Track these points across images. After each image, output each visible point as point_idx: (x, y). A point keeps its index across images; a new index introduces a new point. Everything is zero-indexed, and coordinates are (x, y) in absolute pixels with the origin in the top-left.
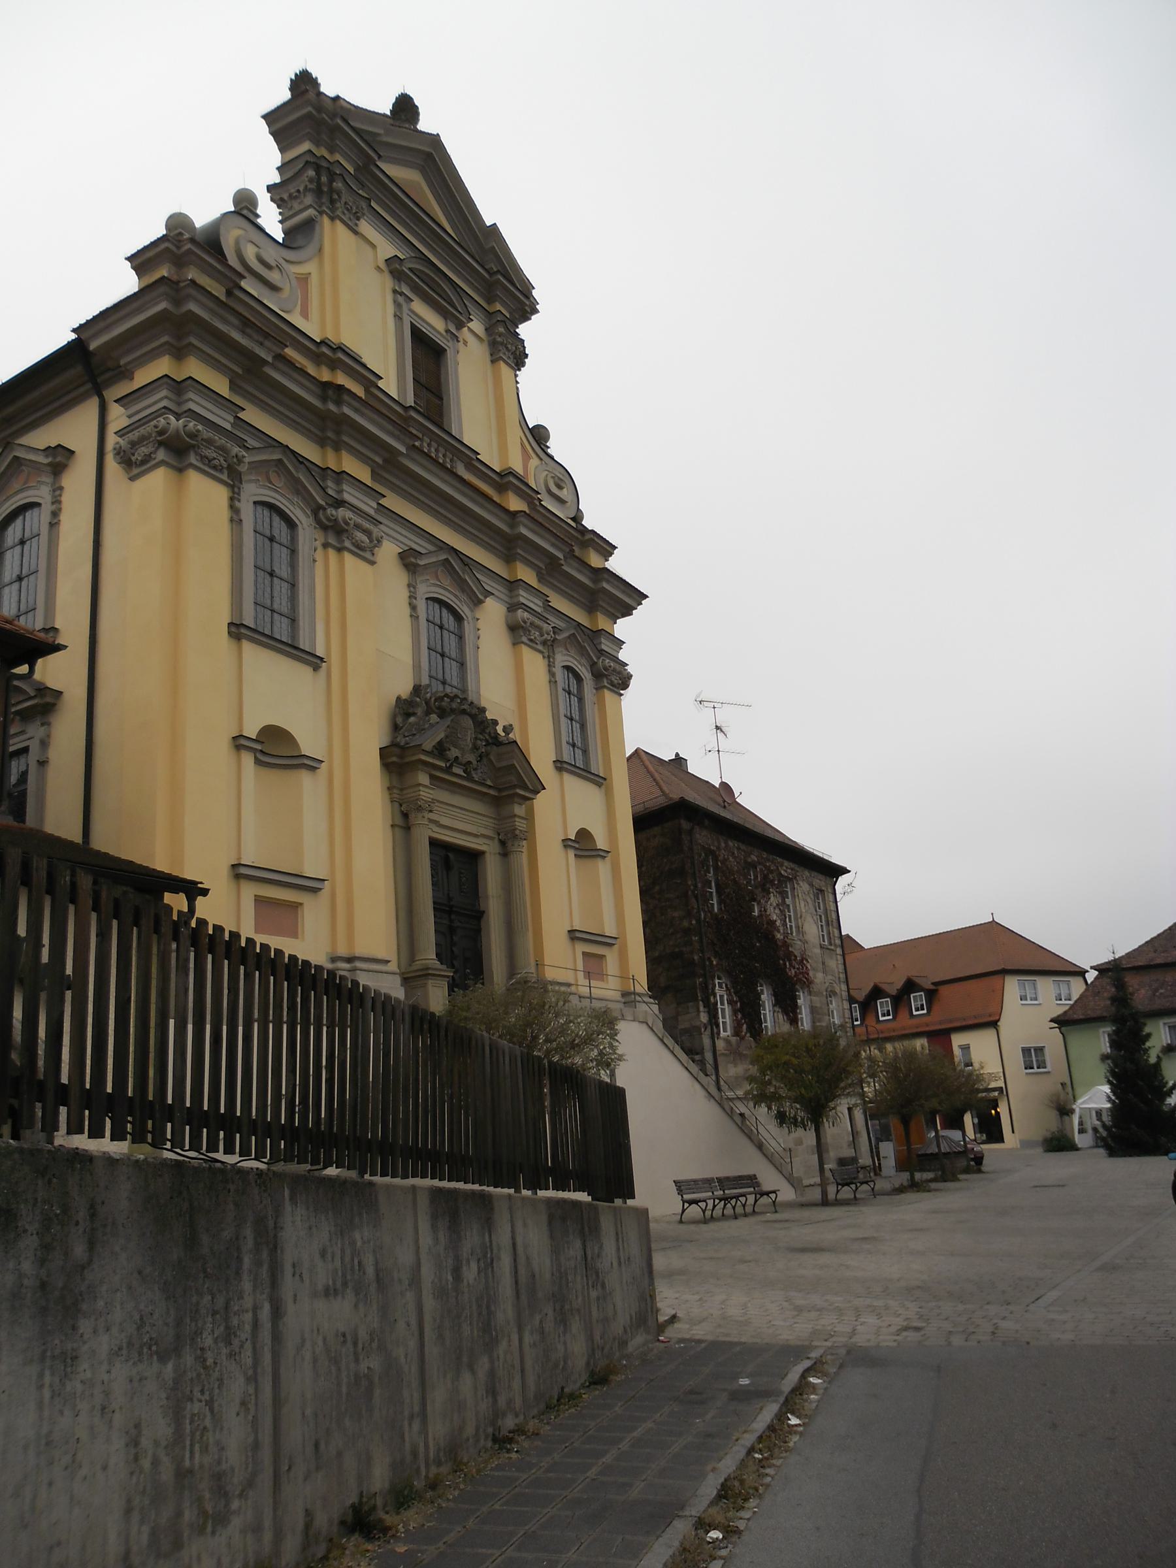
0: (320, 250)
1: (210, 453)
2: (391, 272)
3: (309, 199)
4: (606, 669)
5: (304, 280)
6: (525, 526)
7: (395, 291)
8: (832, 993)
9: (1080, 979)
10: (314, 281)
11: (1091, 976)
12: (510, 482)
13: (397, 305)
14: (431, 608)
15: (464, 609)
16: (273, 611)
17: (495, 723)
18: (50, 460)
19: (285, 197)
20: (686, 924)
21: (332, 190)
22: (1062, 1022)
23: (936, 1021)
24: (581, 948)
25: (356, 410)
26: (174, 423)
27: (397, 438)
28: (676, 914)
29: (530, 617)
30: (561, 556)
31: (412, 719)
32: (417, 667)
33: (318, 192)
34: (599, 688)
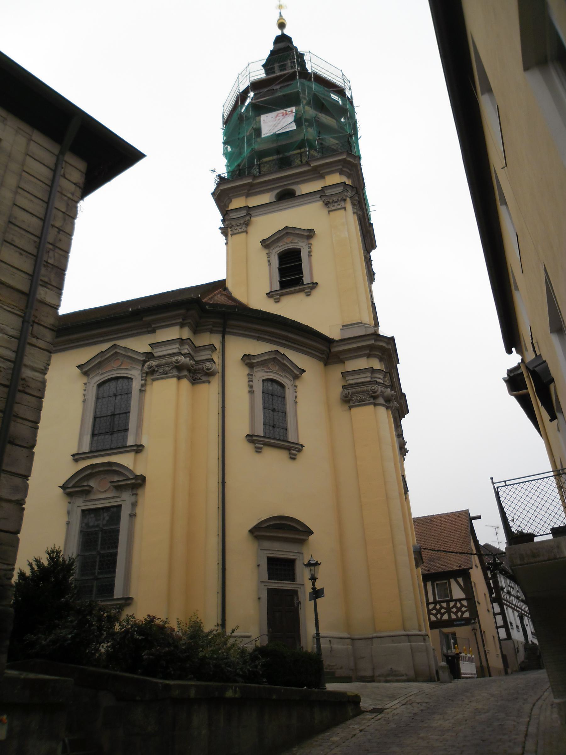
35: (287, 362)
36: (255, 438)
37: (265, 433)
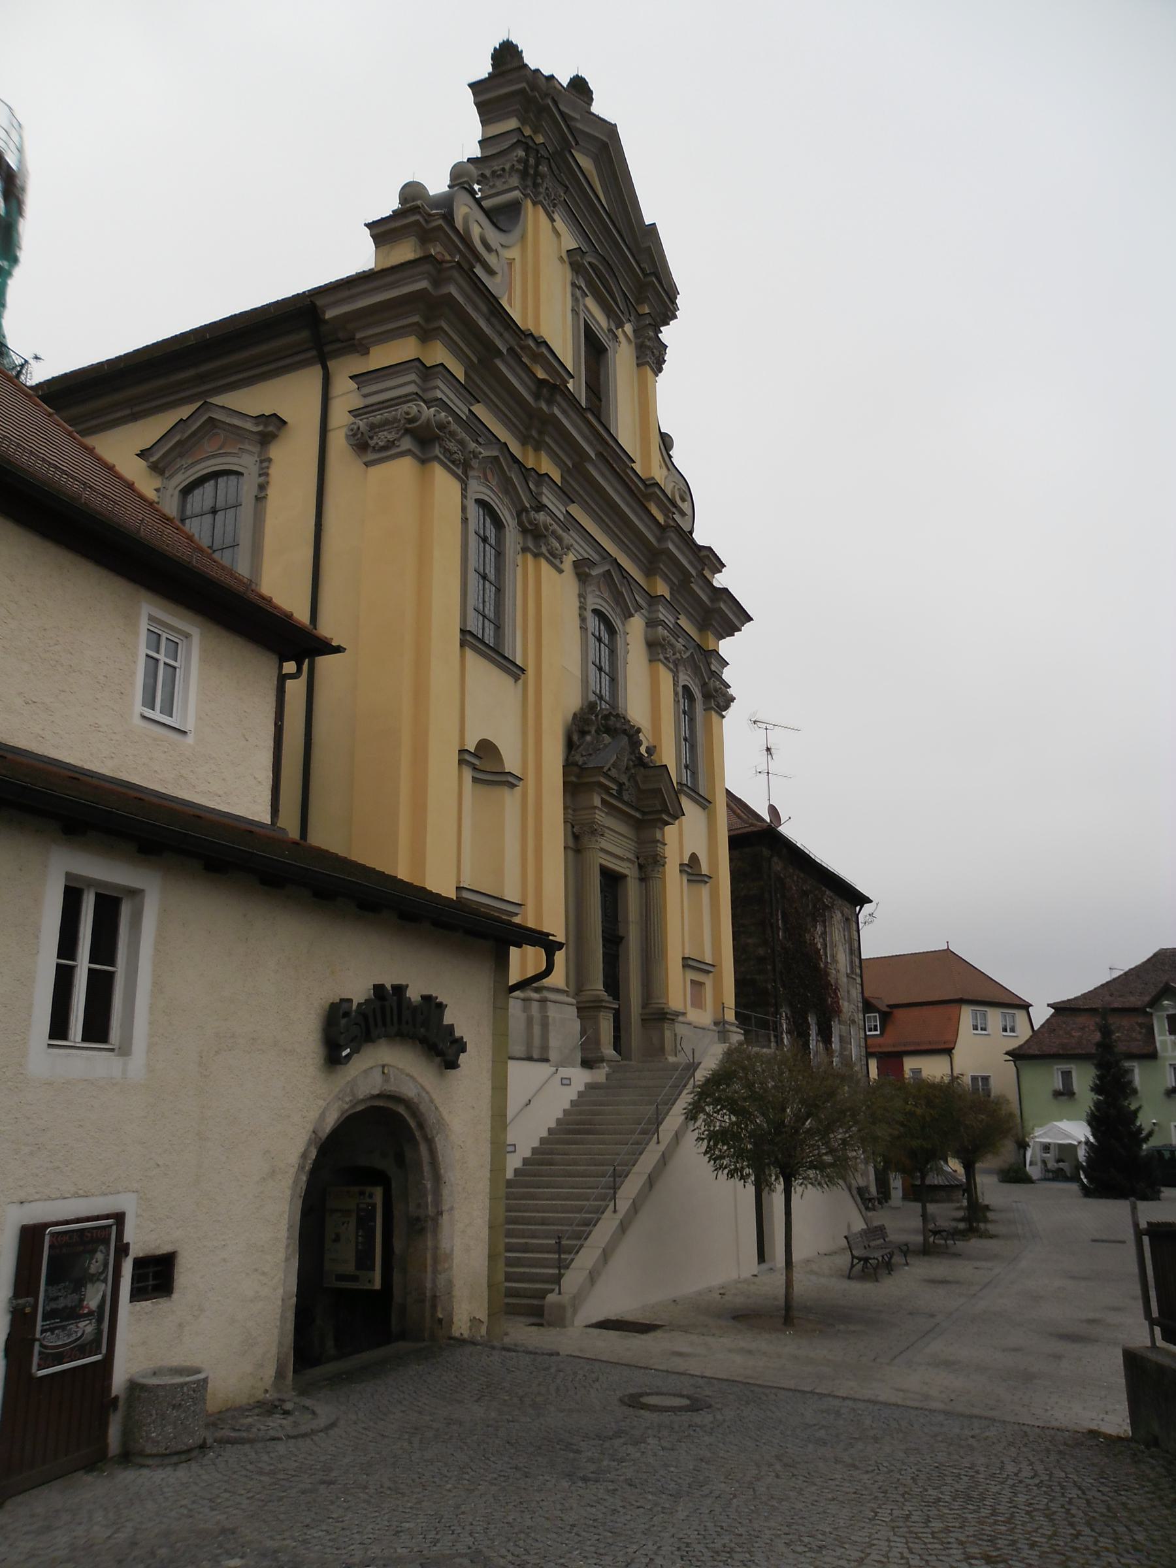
0: (523, 237)
1: (452, 446)
2: (571, 264)
3: (515, 181)
4: (716, 691)
5: (510, 263)
6: (673, 542)
7: (573, 284)
8: (853, 1022)
9: (1024, 1012)
10: (517, 265)
11: (1041, 1015)
13: (575, 299)
15: (617, 622)
16: (484, 616)
18: (260, 428)
19: (488, 173)
20: (761, 951)
21: (537, 174)
22: (1017, 1056)
23: (889, 1043)
24: (692, 975)
26: (428, 413)
28: (749, 941)
31: (588, 738)
32: (585, 682)
33: (524, 174)
34: (707, 709)
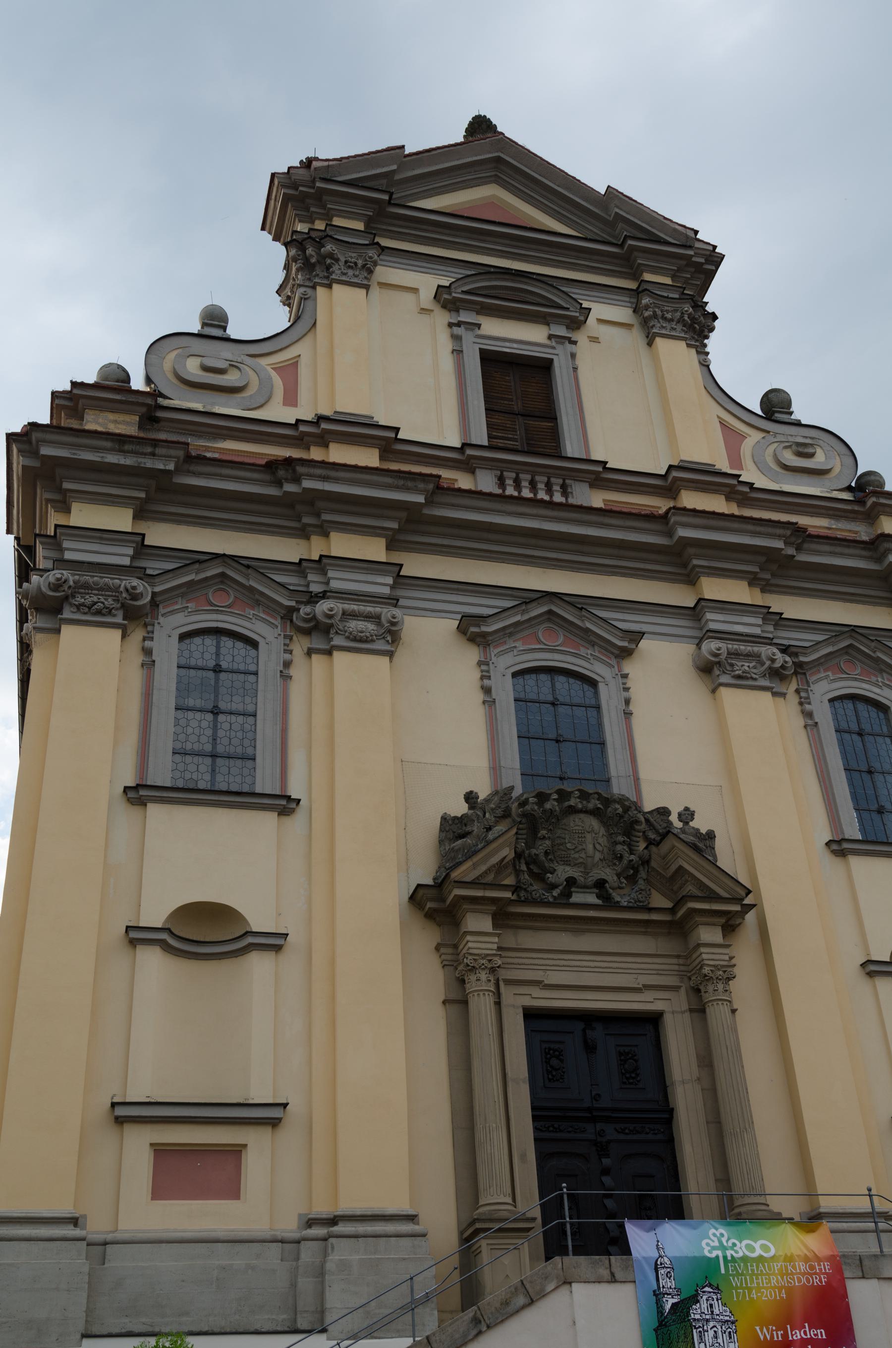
2: (444, 307)
12: (676, 479)
13: (456, 338)
14: (841, 711)
15: (598, 669)
17: (664, 812)
25: (325, 479)
27: (407, 489)
29: (722, 645)
30: (779, 544)
35: (595, 624)
36: (846, 845)
37: (863, 829)
